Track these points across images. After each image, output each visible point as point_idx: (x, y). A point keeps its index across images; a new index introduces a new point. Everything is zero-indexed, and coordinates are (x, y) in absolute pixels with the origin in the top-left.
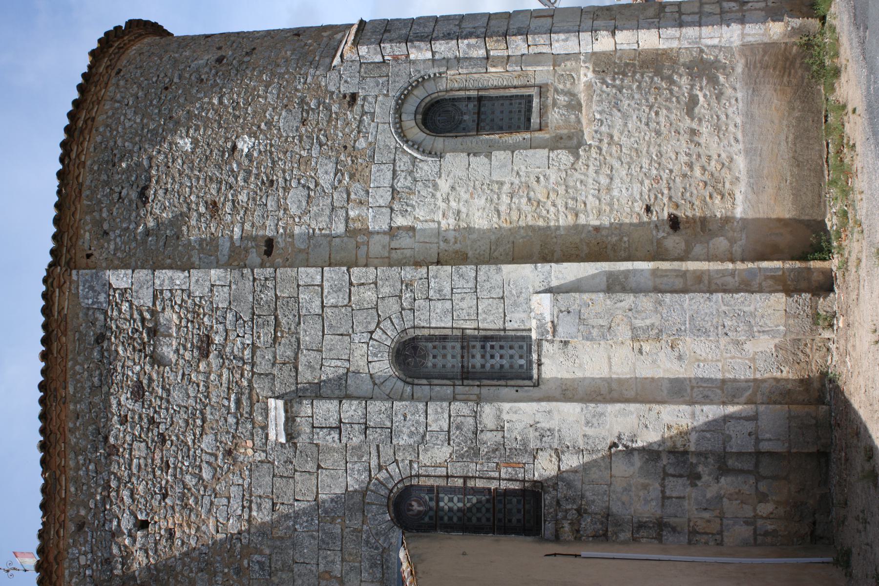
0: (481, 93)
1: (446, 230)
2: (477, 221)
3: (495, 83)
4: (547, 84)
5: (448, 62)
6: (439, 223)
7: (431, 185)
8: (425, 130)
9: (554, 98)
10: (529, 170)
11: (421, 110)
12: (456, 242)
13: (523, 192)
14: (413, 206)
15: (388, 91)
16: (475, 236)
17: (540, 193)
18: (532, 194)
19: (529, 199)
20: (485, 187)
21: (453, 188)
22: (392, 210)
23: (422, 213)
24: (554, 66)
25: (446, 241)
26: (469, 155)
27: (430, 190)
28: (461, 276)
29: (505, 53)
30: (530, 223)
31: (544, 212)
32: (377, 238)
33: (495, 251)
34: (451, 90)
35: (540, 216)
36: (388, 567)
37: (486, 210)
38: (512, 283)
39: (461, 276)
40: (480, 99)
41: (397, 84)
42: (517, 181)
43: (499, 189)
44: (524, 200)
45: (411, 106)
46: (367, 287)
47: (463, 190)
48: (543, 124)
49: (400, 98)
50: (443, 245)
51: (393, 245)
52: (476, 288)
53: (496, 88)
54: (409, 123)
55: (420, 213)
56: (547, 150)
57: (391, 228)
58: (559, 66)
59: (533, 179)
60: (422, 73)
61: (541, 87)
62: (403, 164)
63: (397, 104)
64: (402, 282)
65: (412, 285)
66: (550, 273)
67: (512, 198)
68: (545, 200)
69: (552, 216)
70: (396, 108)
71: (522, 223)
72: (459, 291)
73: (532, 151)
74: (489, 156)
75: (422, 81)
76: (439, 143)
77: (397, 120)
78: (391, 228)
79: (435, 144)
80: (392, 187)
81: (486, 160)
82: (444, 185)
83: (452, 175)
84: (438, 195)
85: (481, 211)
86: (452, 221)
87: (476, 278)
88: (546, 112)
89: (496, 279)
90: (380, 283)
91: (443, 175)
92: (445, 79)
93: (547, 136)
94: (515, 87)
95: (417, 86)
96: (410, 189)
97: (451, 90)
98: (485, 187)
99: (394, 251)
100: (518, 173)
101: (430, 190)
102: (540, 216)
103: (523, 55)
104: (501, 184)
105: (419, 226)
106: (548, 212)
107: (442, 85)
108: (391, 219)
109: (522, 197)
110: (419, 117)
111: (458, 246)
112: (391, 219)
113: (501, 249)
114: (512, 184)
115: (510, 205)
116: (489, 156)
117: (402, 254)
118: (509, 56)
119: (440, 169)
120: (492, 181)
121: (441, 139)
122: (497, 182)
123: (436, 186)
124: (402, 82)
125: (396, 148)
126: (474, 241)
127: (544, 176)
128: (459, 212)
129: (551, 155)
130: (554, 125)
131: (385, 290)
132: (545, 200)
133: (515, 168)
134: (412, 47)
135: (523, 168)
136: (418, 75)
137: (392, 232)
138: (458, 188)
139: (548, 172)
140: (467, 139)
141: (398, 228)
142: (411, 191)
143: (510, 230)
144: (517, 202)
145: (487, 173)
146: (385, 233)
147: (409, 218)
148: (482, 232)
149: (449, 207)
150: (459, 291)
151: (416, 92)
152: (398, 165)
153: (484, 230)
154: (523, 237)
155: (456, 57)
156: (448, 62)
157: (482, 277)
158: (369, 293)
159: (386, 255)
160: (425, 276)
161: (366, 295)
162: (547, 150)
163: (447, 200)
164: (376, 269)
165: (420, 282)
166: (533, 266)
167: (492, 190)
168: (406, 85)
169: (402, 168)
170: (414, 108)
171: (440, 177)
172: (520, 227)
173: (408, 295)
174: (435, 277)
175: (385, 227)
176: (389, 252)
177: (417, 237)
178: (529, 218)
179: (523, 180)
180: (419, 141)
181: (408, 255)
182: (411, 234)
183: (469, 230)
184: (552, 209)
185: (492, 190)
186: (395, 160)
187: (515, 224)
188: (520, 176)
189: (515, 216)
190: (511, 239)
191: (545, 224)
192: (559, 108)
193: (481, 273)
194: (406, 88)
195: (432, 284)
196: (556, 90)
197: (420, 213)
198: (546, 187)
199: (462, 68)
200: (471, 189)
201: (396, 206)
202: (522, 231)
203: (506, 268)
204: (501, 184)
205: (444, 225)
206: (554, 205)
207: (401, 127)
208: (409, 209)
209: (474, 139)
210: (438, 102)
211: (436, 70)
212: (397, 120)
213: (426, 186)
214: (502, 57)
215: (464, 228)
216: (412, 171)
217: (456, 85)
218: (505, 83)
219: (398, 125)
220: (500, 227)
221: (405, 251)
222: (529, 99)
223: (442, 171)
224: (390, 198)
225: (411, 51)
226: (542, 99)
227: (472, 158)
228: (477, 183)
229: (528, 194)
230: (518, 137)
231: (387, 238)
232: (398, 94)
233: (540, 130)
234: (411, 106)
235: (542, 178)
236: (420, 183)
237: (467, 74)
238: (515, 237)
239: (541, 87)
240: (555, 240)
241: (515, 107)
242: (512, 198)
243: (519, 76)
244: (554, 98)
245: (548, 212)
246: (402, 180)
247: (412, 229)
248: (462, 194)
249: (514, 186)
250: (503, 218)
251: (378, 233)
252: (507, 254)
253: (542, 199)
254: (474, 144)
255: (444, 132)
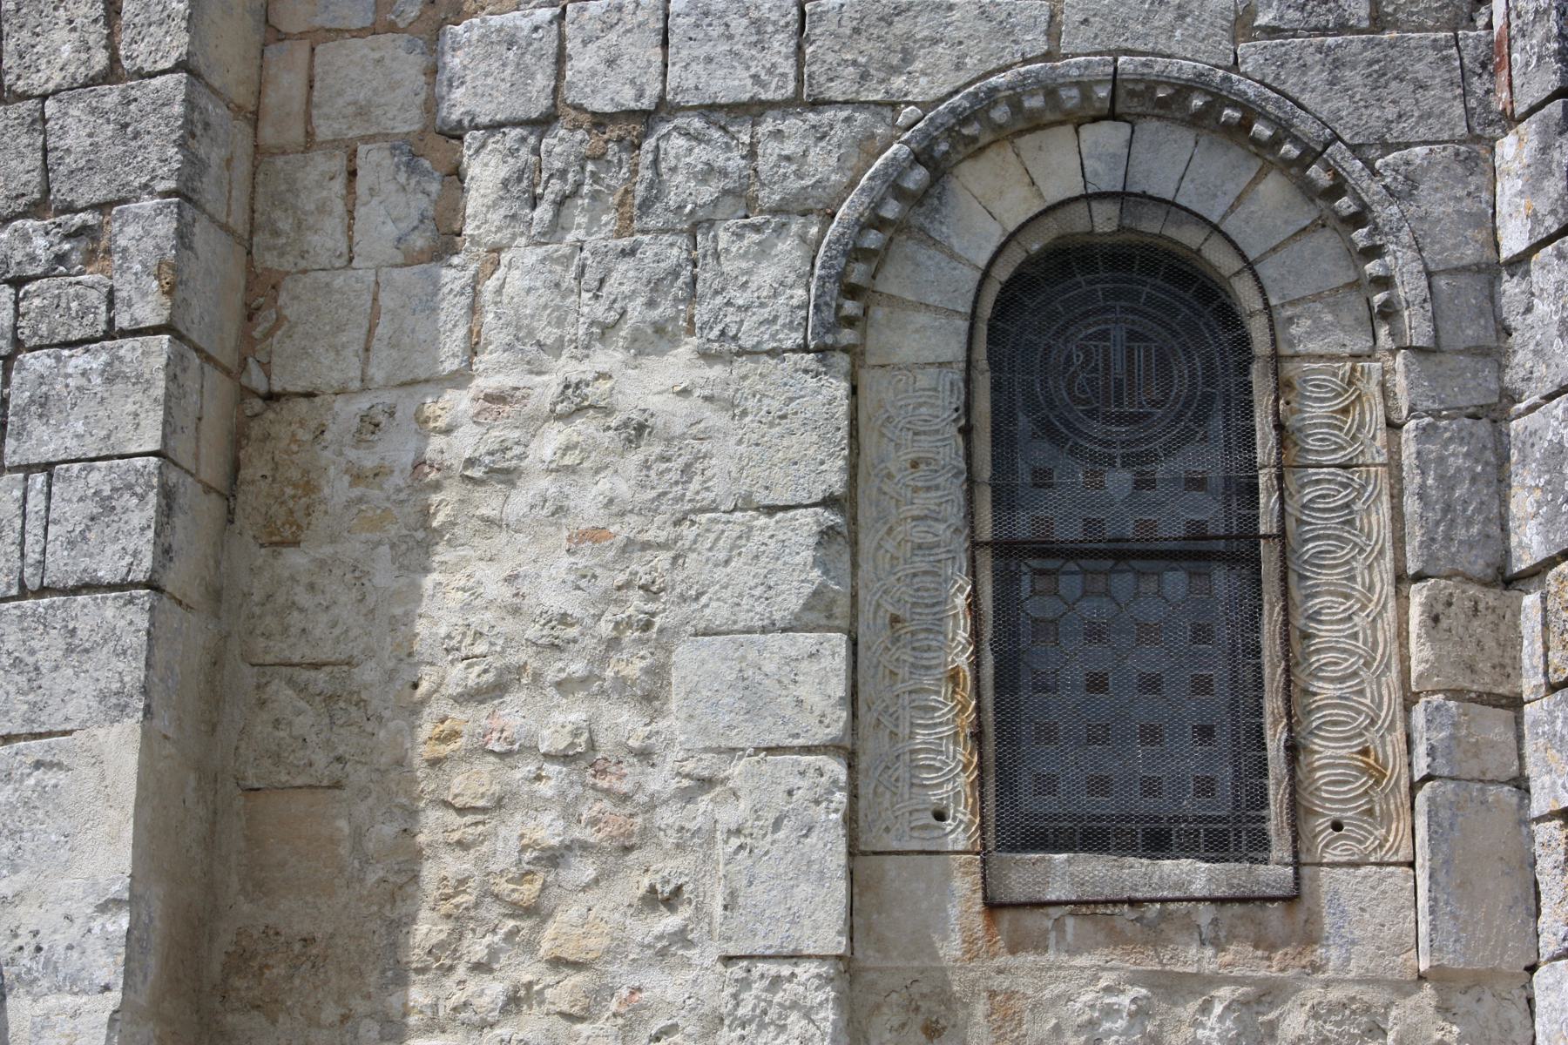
0: (1268, 555)
1: (421, 421)
2: (460, 580)
4: (1310, 937)
5: (1480, 352)
6: (460, 379)
7: (664, 309)
8: (1015, 256)
9: (1215, 981)
10: (722, 850)
11: (1151, 224)
12: (358, 477)
13: (598, 819)
14: (555, 229)
15: (1272, 32)
16: (383, 575)
17: (587, 915)
18: (584, 869)
19: (553, 858)
20: (636, 603)
21: (638, 431)
22: (543, 123)
23: (516, 281)
24: (1438, 977)
25: (370, 425)
26: (829, 502)
27: (636, 310)
28: (107, 506)
29: (1530, 683)
30: (430, 873)
31: (477, 948)
32: (409, 68)
33: (302, 690)
34: (1283, 387)
35: (460, 922)
37: (509, 625)
38: (50, 778)
39: (107, 506)
40: (1241, 550)
41: (1317, 77)
42: (660, 780)
43: (622, 683)
44: (548, 830)
45: (1171, 164)
46: (97, 34)
47: (624, 489)
48: (1031, 920)
49: (1218, 99)
50: (349, 410)
51: (372, 160)
52: (43, 591)
53: (1294, 639)
55: (521, 275)
56: (839, 945)
57: (455, 134)
58: (1444, 1010)
59: (667, 868)
60: (1388, 212)
61: (1291, 900)
62: (799, 154)
63: (1183, 89)
64: (102, 207)
65: (90, 257)
66: (74, 985)
67: (564, 758)
68: (546, 947)
69: (454, 992)
70: (1152, 85)
71: (433, 825)
72: (36, 502)
73: (837, 860)
74: (816, 613)
75: (1337, 211)
76: (927, 337)
77: (1071, 96)
78: (455, 134)
79: (922, 318)
80: (663, 109)
81: (791, 602)
82: (658, 384)
83: (714, 418)
84: (606, 358)
85: (507, 592)
86: (466, 443)
87: (90, 586)
88: (1116, 938)
89: (74, 694)
90: (111, 96)
91: (717, 371)
92: (1362, 343)
93: (951, 949)
94: (1293, 750)
95: (1308, 190)
96: (646, 206)
97: (1283, 387)
98: (636, 603)
99: (338, 163)
100: (706, 783)
101: (636, 310)
102: (460, 922)
103: (1521, 784)
104: (651, 697)
105: (452, 277)
106: (479, 968)
107: (1318, 336)
108: (495, 127)
109: (569, 813)
110: (1105, 219)
111: (337, 489)
112: (495, 127)
113: (306, 721)
114: (645, 754)
115: (530, 749)
116: (816, 613)
117: (322, 209)
118: (1515, 703)
119: (753, 353)
120: (666, 641)
121: (954, 349)
122: (658, 672)
123: (660, 336)
124: (1325, 98)
125: (894, 106)
126: (359, 575)
127: (681, 937)
128: (508, 476)
129: (806, 971)
130: (1025, 984)
131: (75, 128)
132: (546, 947)
133: (736, 770)
134: (1544, 132)
135: (729, 815)
136: (1372, 190)
137: (438, 145)
138: (635, 458)
139: (705, 955)
140: (956, 490)
141: (456, 174)
142: (636, 210)
143: (401, 762)
144: (546, 789)
145: (717, 612)
146: (432, 105)
147: (496, 217)
148: (396, 618)
149: (534, 423)
150: (36, 502)
151: (1273, 188)
152: (792, 124)
153: (408, 619)
154: (358, 835)
155: (1511, 397)
156: (1480, 352)
157: (89, 613)
158: (66, 51)
159: (324, 131)
160: (123, 321)
161: (60, 35)
162: (839, 945)
163: (575, 403)
164: (179, 67)
165: (95, 297)
166: (120, 888)
167: (613, 643)
168: (1307, 128)
169: (770, 151)
170: (1163, 187)
171: (705, 356)
172: (413, 814)
173: (40, 242)
174: (111, 376)
175: (459, 103)
176: (335, 143)
177: (400, 275)
178: (453, 865)
179: (667, 816)
180: (941, 231)
181: (314, 239)
182: (419, 241)
183: (419, 543)
184: (493, 990)
185: (613, 643)
186: (817, 104)
187: (427, 785)
188: (687, 796)
189: (470, 783)
190: (358, 775)
191: (416, 957)
192: (1141, 1012)
193: (109, 609)
194: (1284, 132)
195: (79, 360)
196: (1268, 994)
197: (521, 275)
198: (615, 951)
199: (1425, 433)
200: (621, 531)
201: (560, 144)
202: (389, 830)
203: (119, 748)
204: (651, 697)
205: (459, 402)
206: (514, 1002)
207: (1035, 124)
208: (543, 212)
209: (947, 532)
210: (1229, 316)
211: (1409, 287)
212: (1071, 96)
213: (656, 286)
214: (1509, 667)
215: (426, 514)
216: (751, 205)
217: (1316, 412)
218: (1326, 690)
219: (1035, 102)
220: (415, 709)
221: (333, 225)
222: (1231, 837)
223: (744, 366)
224: (600, 104)
225: (1529, 128)
226: (1205, 914)
227: (808, 522)
228: (663, 559)
229: (585, 847)
230: (947, 771)
231: (407, 122)
232: (1250, 89)
233: (993, 907)
234: (1171, 164)
235: (669, 922)
236: (676, 254)
237: (1394, 466)
238: (363, 793)
240: (330, 1013)
242: (564, 758)
243: (1377, 773)
244: (1215, 981)
245: (479, 968)
246: (701, 154)
247: (446, 242)
248: (604, 484)
249: (632, 768)
250: (460, 717)
251: (433, 71)
252: (277, 758)
253: (550, 930)
254: (919, 534)
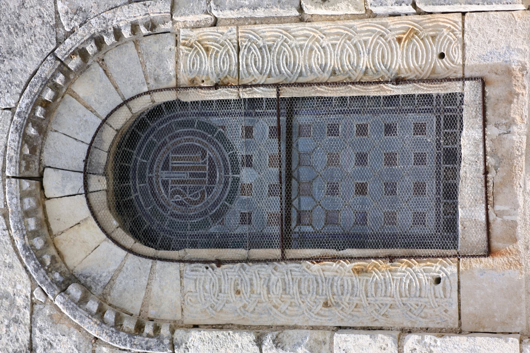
0: (288, 93)
3: (332, 62)
11: (102, 157)
34: (193, 85)
36: (325, 256)
48: (497, 229)
54: (69, 208)
60: (95, 26)
61: (484, 83)
63: (25, 139)
77: (29, 203)
79: (155, 287)
88: (509, 180)
95: (82, 69)
110: (99, 183)
121: (173, 269)
151: (82, 88)
207: (45, 222)
210: (156, 112)
212: (29, 203)
218: (365, 61)
219: (32, 223)
230: (414, 274)
233: (489, 252)
239: (484, 83)
241: (405, 141)
243: (412, 33)
255: (181, 246)
